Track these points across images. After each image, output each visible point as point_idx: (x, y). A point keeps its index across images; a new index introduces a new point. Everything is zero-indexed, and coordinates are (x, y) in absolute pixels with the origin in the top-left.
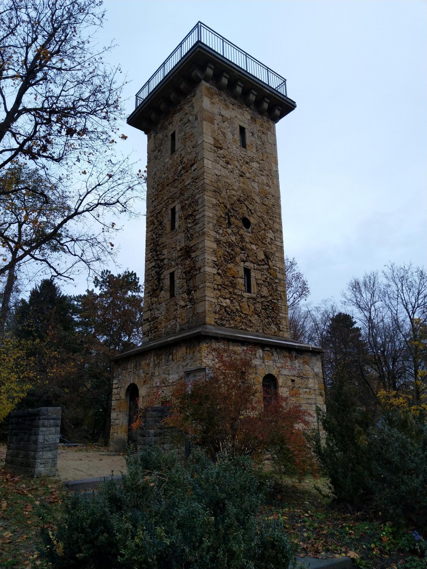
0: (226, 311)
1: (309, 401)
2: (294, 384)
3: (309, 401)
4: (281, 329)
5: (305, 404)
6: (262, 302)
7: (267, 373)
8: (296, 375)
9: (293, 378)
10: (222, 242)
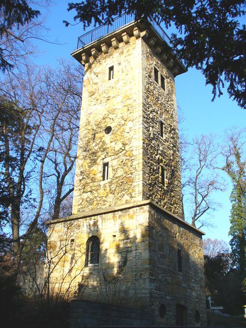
6: (117, 182)
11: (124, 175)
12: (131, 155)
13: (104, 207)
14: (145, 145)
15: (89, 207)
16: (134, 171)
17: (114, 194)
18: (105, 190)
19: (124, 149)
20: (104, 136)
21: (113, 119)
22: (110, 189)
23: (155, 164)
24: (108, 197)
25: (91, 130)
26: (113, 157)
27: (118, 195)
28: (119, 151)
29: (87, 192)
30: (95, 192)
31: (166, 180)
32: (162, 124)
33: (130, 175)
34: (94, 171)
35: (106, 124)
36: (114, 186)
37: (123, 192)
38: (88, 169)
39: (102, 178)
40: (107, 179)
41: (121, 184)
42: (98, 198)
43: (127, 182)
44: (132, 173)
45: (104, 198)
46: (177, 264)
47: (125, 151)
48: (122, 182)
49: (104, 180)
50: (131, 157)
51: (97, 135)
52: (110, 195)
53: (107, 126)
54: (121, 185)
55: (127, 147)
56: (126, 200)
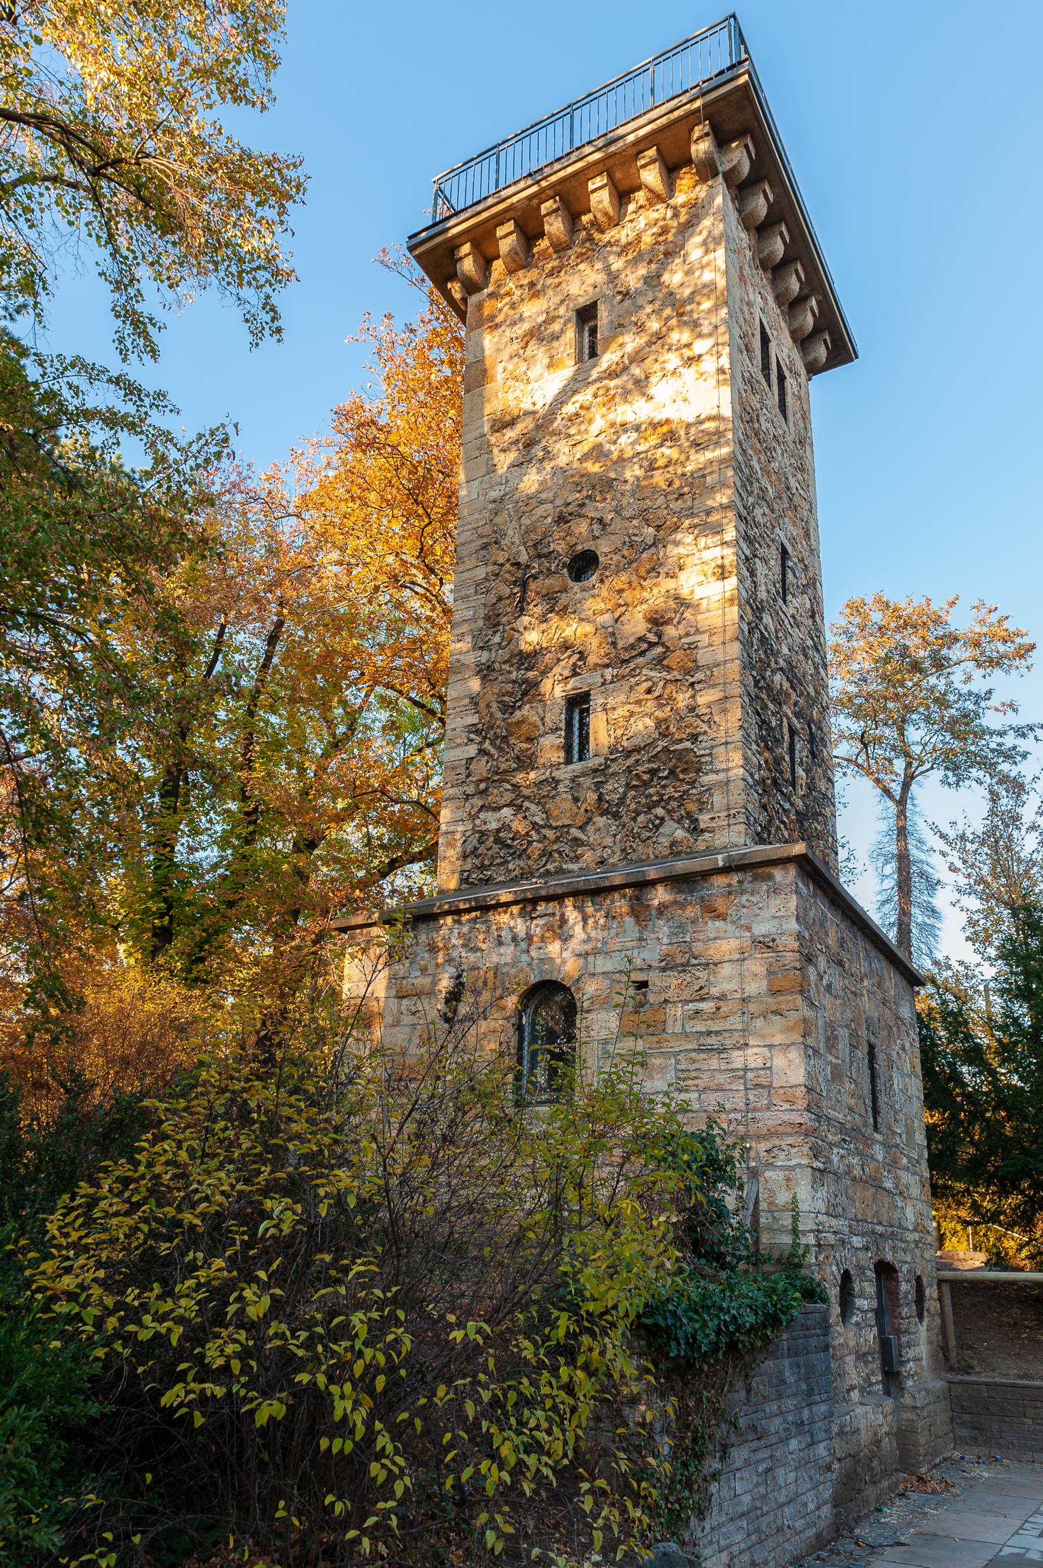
0: (498, 841)
1: (713, 1040)
2: (645, 995)
3: (713, 1040)
4: (702, 826)
5: (694, 1055)
6: (629, 769)
7: (533, 980)
8: (655, 964)
9: (641, 977)
10: (497, 666)
11: (661, 744)
12: (690, 664)
13: (571, 866)
14: (746, 628)
15: (511, 866)
16: (705, 727)
17: (616, 816)
18: (576, 800)
19: (652, 638)
20: (565, 590)
21: (601, 521)
22: (600, 799)
23: (771, 706)
24: (590, 828)
25: (508, 566)
26: (609, 673)
27: (634, 819)
28: (632, 647)
29: (499, 808)
30: (533, 807)
31: (800, 772)
32: (784, 554)
33: (687, 744)
34: (525, 727)
35: (572, 540)
36: (614, 788)
37: (660, 811)
38: (499, 715)
39: (562, 754)
40: (580, 759)
41: (646, 777)
42: (550, 834)
43: (672, 772)
44: (694, 738)
45: (575, 832)
46: (869, 1102)
47: (660, 650)
48: (653, 772)
49: (568, 761)
50: (688, 672)
51: (533, 585)
52: (600, 821)
53: (579, 547)
54: (646, 784)
55: (670, 631)
56: (673, 844)
